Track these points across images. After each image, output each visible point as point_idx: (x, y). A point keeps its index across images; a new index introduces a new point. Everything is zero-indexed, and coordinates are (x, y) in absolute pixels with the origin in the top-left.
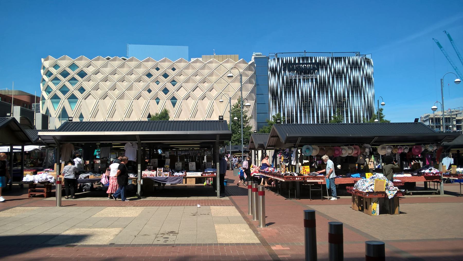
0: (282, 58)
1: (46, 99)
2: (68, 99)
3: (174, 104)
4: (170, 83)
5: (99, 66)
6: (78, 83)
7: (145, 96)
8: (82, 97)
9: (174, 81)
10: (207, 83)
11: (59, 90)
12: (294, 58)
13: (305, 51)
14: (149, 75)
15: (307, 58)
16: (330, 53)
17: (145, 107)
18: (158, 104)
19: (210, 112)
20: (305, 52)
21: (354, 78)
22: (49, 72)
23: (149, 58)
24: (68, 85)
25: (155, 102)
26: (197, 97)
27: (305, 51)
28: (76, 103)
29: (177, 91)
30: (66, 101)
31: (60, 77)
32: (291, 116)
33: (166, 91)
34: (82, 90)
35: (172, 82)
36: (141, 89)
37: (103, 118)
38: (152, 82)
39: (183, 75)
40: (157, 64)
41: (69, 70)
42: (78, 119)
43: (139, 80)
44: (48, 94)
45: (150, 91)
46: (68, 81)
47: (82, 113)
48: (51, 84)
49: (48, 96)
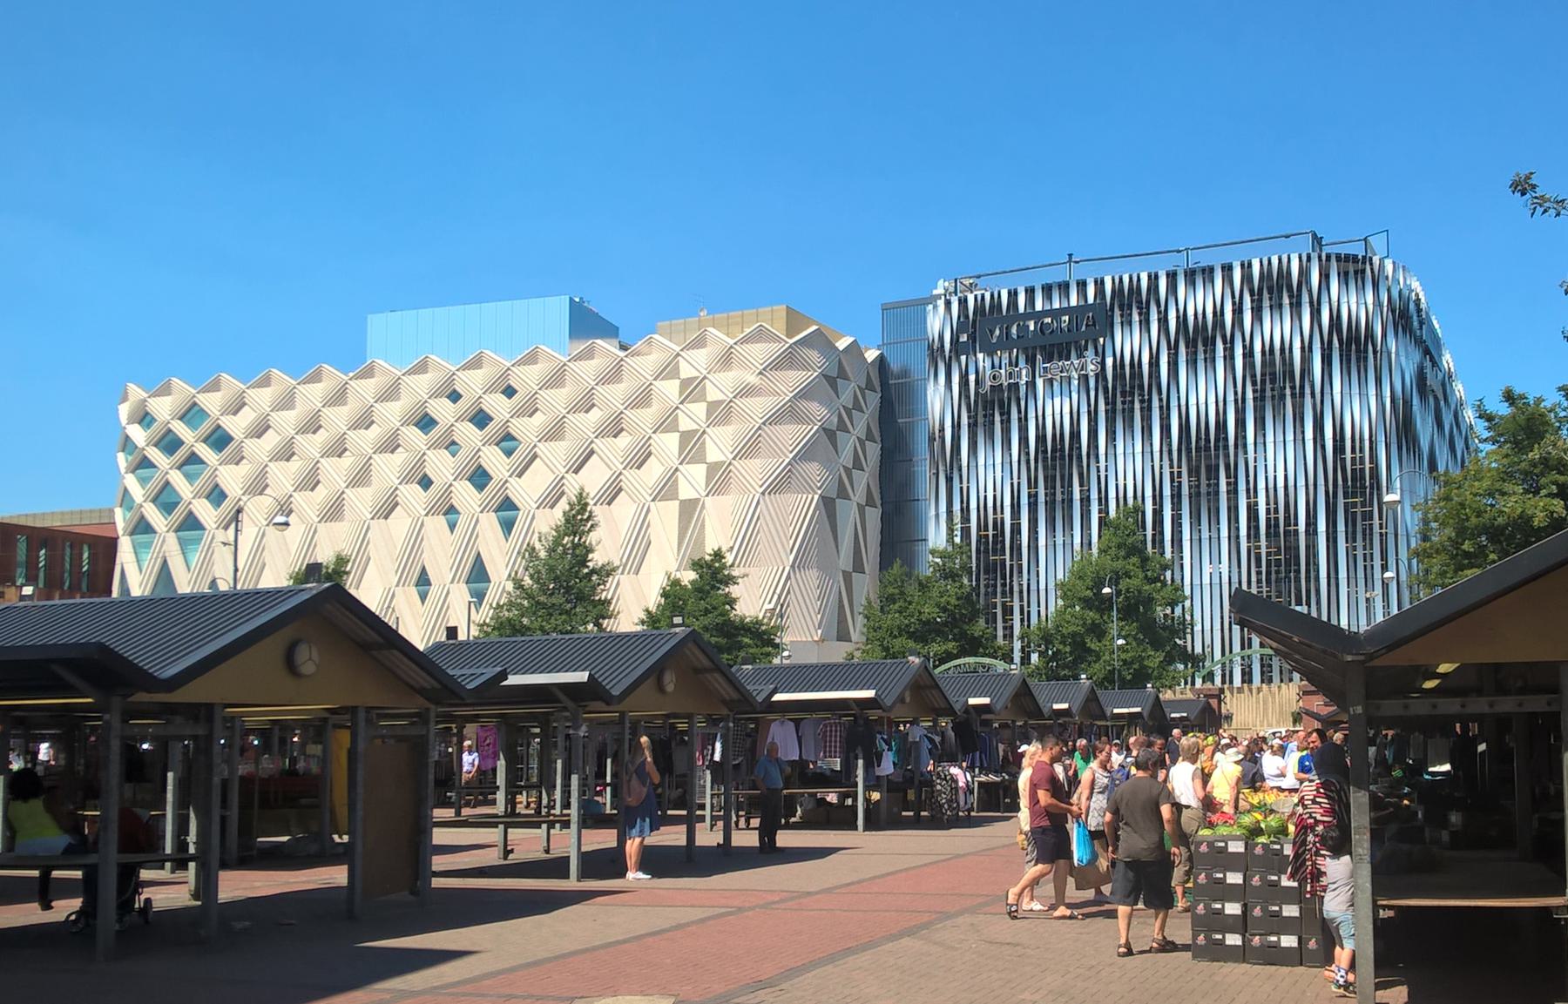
0: (1135, 279)
1: (157, 528)
2: (176, 531)
3: (508, 526)
4: (497, 444)
5: (762, 365)
6: (207, 473)
7: (464, 501)
8: (763, 485)
9: (509, 437)
10: (629, 433)
11: (154, 501)
12: (1261, 262)
13: (1070, 255)
14: (426, 422)
15: (1064, 288)
16: (1179, 251)
17: (631, 537)
18: (452, 532)
19: (467, 560)
20: (1070, 261)
21: (1268, 352)
22: (170, 435)
23: (537, 347)
24: (177, 479)
25: (441, 521)
26: (404, 508)
27: (1070, 255)
28: (150, 548)
29: (520, 475)
30: (172, 540)
31: (204, 451)
32: (1354, 532)
33: (480, 478)
34: (216, 495)
35: (503, 444)
36: (788, 450)
37: (382, 589)
38: (434, 446)
39: (599, 408)
40: (451, 379)
41: (180, 429)
42: (464, 585)
43: (391, 445)
44: (166, 515)
45: (426, 483)
46: (176, 468)
47: (427, 568)
48: (177, 479)
49: (166, 523)
